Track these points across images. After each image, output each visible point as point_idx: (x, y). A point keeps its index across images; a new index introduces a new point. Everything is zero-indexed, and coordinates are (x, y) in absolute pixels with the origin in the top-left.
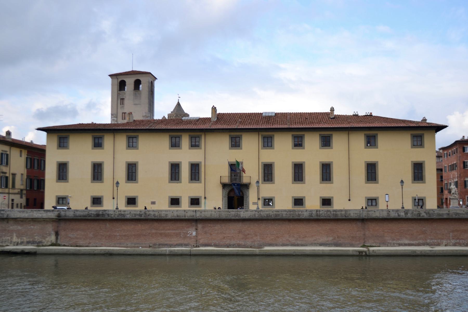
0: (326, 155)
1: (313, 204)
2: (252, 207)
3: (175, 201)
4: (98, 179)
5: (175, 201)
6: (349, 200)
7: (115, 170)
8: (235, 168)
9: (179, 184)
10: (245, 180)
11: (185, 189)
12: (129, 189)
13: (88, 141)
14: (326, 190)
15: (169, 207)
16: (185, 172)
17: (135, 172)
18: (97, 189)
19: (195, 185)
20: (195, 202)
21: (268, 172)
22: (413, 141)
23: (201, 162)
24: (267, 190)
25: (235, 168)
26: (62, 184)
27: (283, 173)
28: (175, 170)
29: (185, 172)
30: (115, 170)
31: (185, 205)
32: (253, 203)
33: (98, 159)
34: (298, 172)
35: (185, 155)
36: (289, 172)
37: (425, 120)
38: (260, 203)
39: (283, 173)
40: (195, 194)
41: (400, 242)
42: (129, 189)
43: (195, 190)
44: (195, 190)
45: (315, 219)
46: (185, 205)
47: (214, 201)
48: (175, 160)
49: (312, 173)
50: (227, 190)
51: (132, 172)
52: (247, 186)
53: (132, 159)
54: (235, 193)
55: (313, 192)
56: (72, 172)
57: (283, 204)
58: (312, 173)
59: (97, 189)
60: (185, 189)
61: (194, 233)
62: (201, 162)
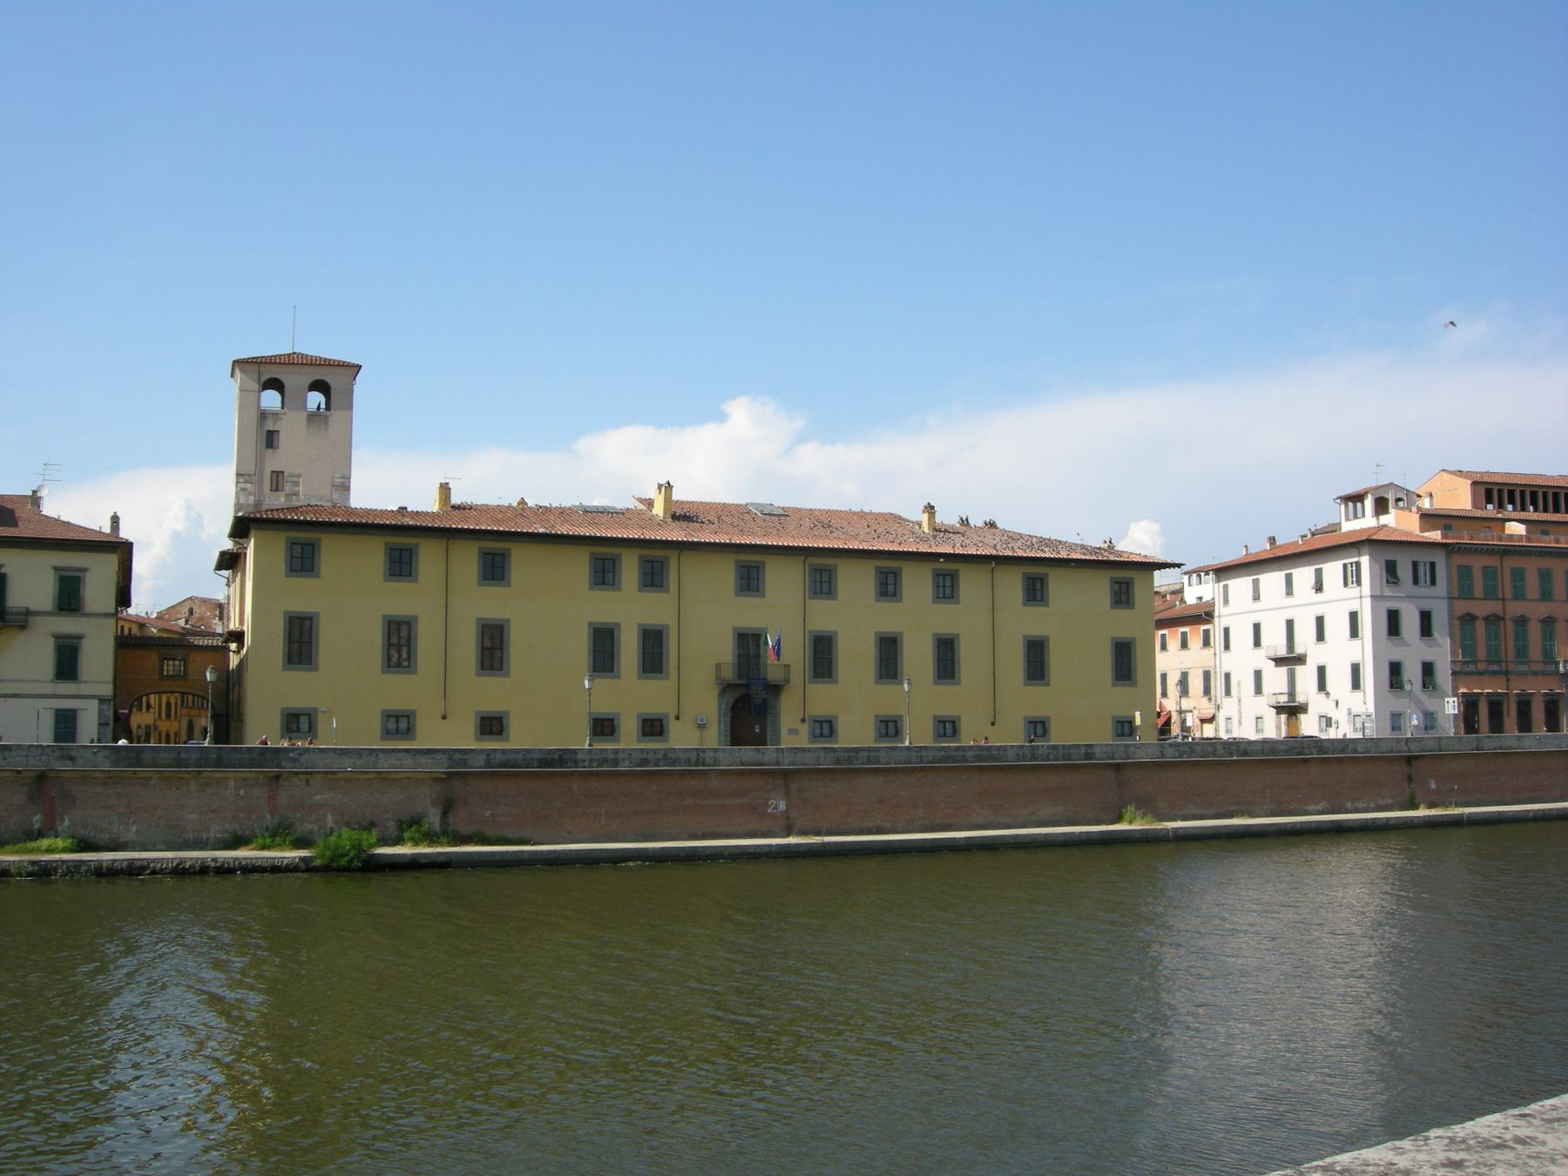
0: (946, 619)
1: (917, 734)
2: (787, 742)
3: (604, 727)
4: (300, 662)
5: (604, 727)
6: (444, 717)
7: (446, 638)
8: (748, 642)
9: (310, 674)
10: (773, 673)
11: (630, 695)
12: (491, 694)
13: (374, 553)
14: (947, 699)
15: (639, 741)
16: (629, 650)
17: (501, 649)
18: (400, 691)
19: (653, 685)
20: (653, 727)
21: (823, 655)
22: (937, 586)
23: (667, 627)
24: (823, 699)
25: (748, 642)
26: (491, 682)
27: (857, 657)
28: (603, 644)
29: (629, 650)
30: (446, 638)
31: (629, 738)
32: (791, 733)
33: (401, 610)
34: (889, 654)
35: (630, 609)
36: (1014, 660)
37: (1111, 547)
38: (804, 729)
39: (857, 657)
40: (652, 709)
41: (1186, 812)
42: (491, 694)
43: (653, 696)
44: (653, 696)
45: (920, 767)
46: (629, 738)
47: (697, 726)
48: (604, 617)
49: (918, 657)
50: (730, 698)
51: (493, 647)
52: (776, 689)
53: (493, 613)
54: (749, 701)
55: (918, 700)
56: (328, 641)
57: (856, 733)
58: (918, 657)
59: (400, 691)
60: (630, 695)
61: (782, 806)
62: (667, 627)
